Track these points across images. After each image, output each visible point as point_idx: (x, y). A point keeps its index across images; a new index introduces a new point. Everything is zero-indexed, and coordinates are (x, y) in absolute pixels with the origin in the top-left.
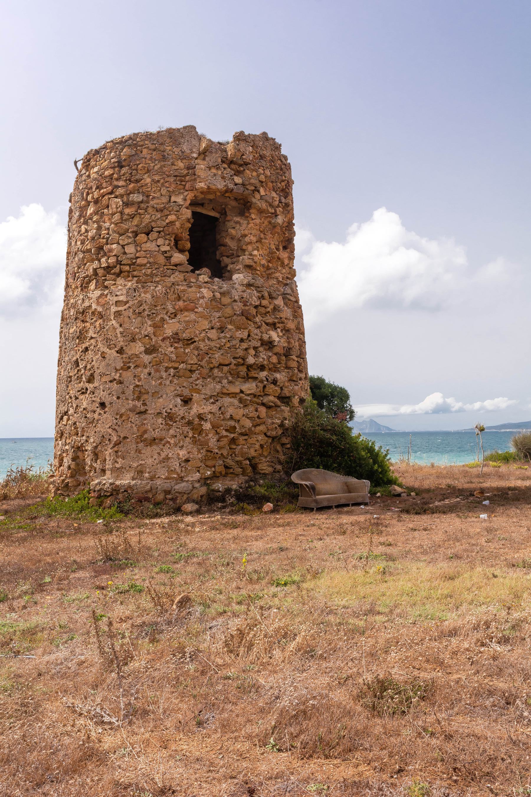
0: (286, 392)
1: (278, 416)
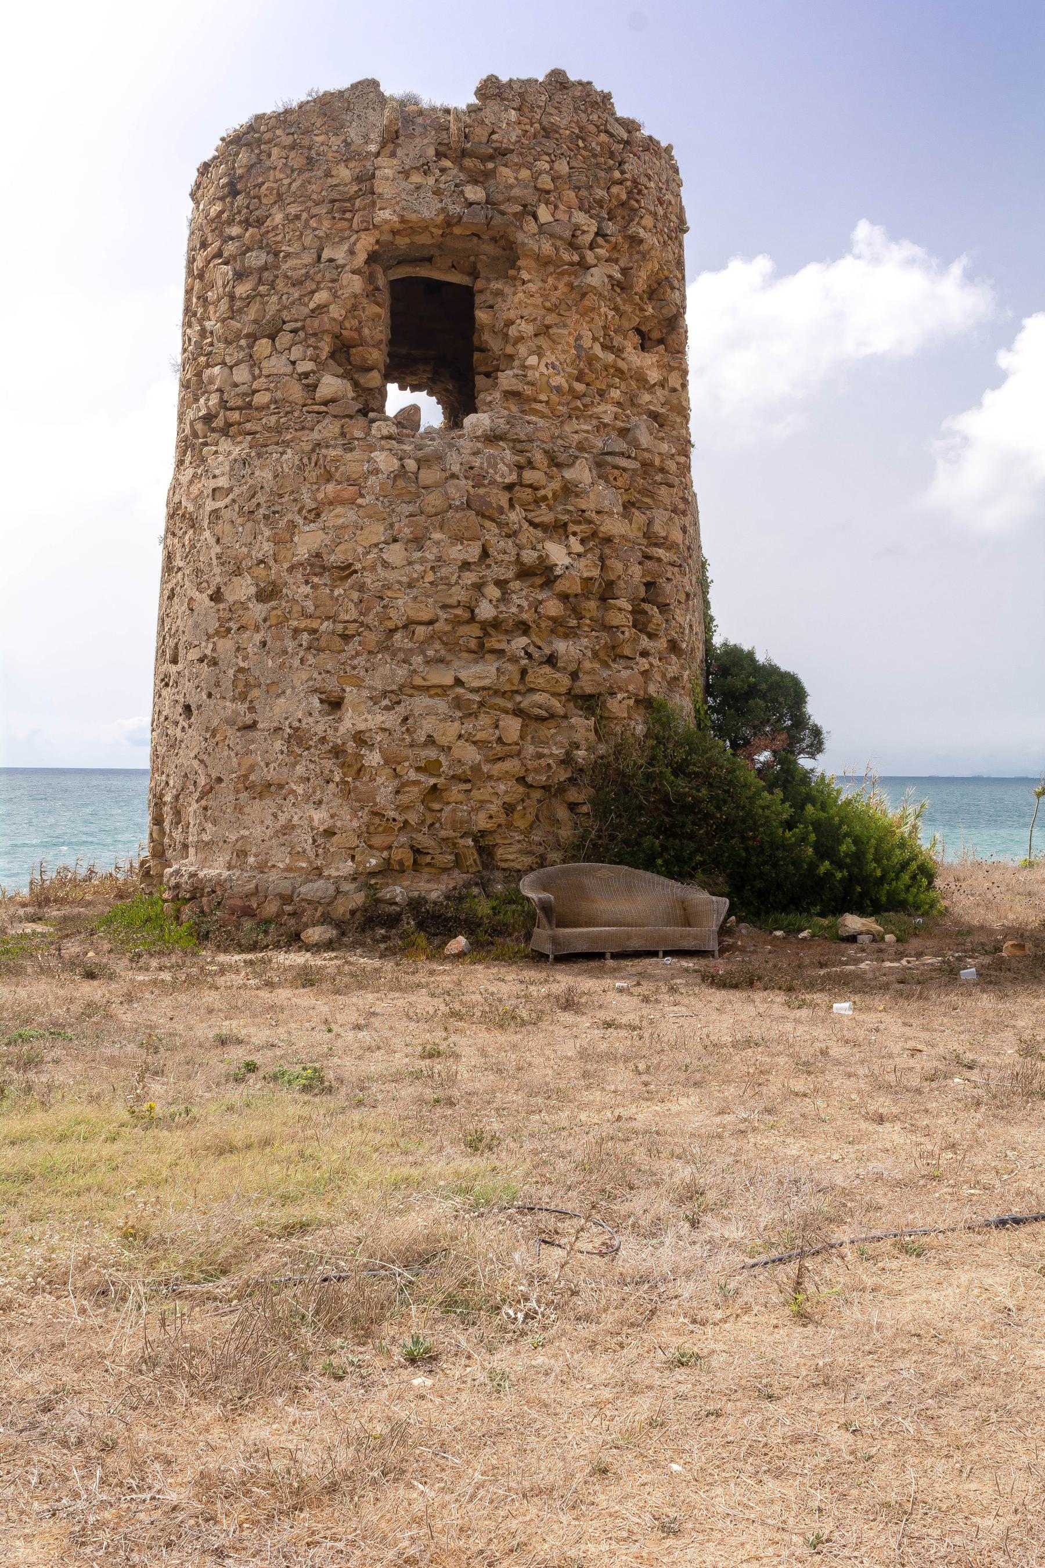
0: (586, 685)
1: (559, 738)
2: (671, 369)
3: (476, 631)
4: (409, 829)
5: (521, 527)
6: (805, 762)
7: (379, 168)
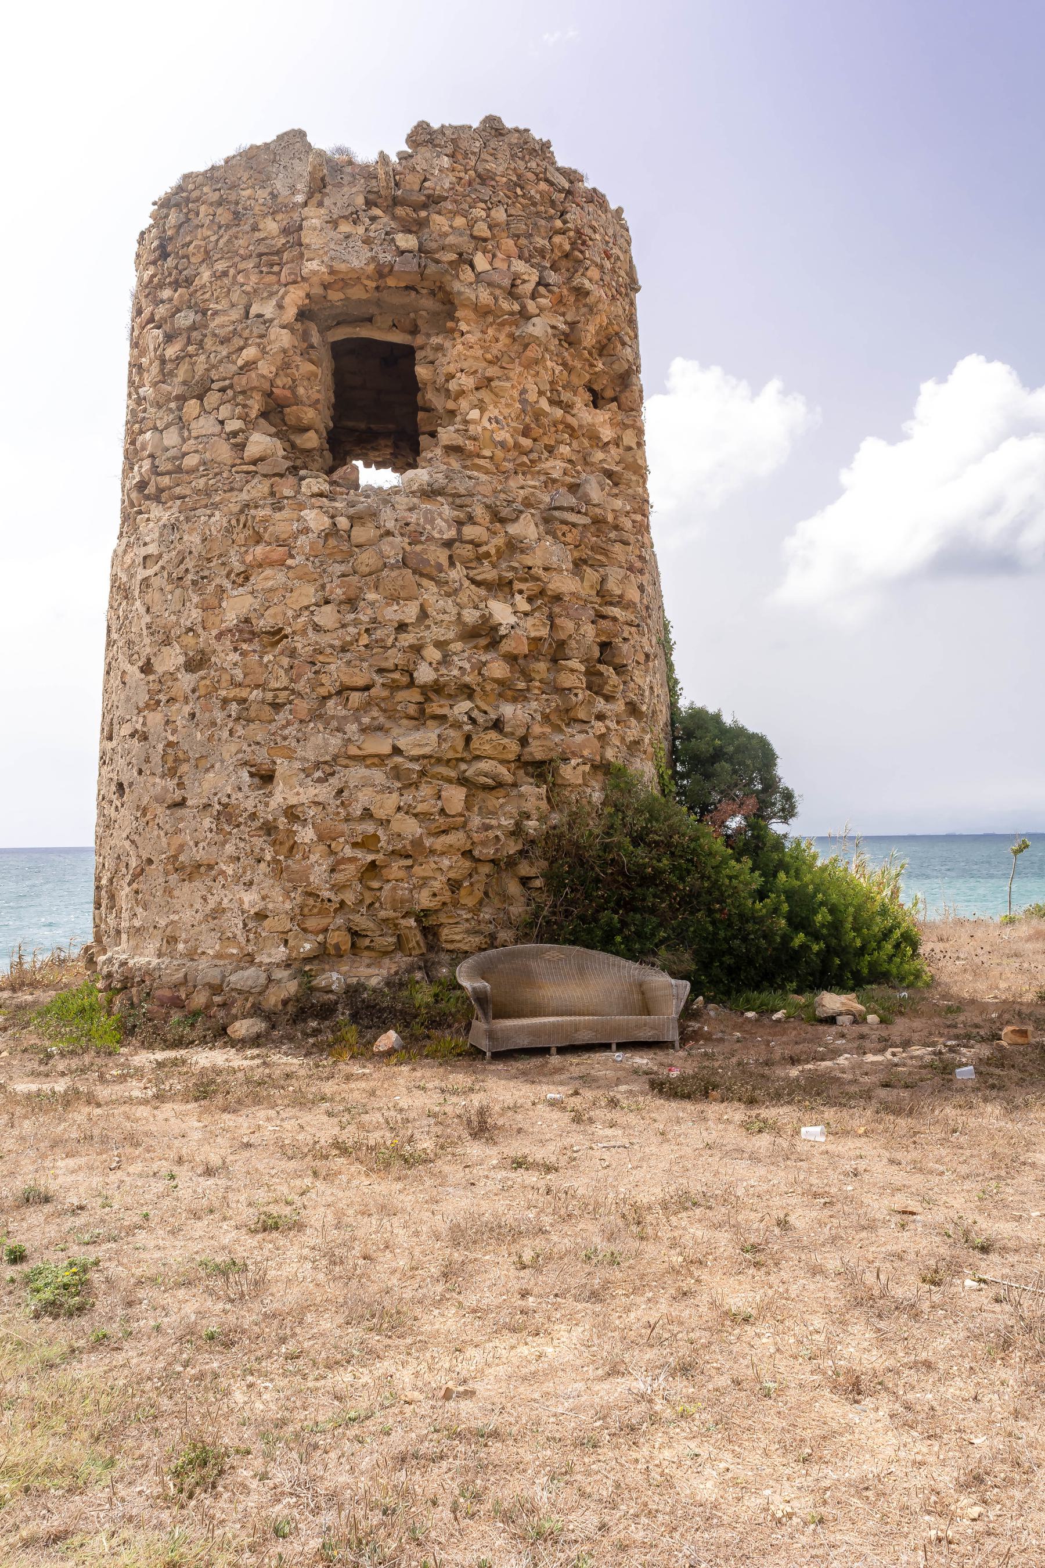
0: (536, 751)
2: (626, 427)
3: (416, 696)
4: (347, 910)
5: (461, 585)
6: (777, 827)
7: (306, 218)
